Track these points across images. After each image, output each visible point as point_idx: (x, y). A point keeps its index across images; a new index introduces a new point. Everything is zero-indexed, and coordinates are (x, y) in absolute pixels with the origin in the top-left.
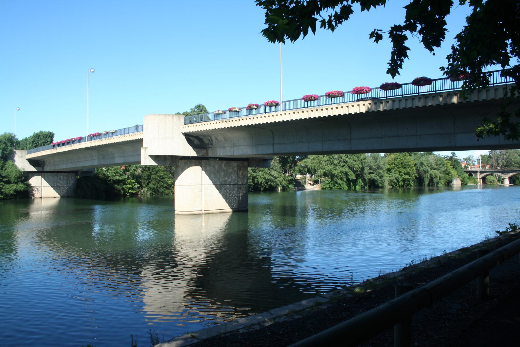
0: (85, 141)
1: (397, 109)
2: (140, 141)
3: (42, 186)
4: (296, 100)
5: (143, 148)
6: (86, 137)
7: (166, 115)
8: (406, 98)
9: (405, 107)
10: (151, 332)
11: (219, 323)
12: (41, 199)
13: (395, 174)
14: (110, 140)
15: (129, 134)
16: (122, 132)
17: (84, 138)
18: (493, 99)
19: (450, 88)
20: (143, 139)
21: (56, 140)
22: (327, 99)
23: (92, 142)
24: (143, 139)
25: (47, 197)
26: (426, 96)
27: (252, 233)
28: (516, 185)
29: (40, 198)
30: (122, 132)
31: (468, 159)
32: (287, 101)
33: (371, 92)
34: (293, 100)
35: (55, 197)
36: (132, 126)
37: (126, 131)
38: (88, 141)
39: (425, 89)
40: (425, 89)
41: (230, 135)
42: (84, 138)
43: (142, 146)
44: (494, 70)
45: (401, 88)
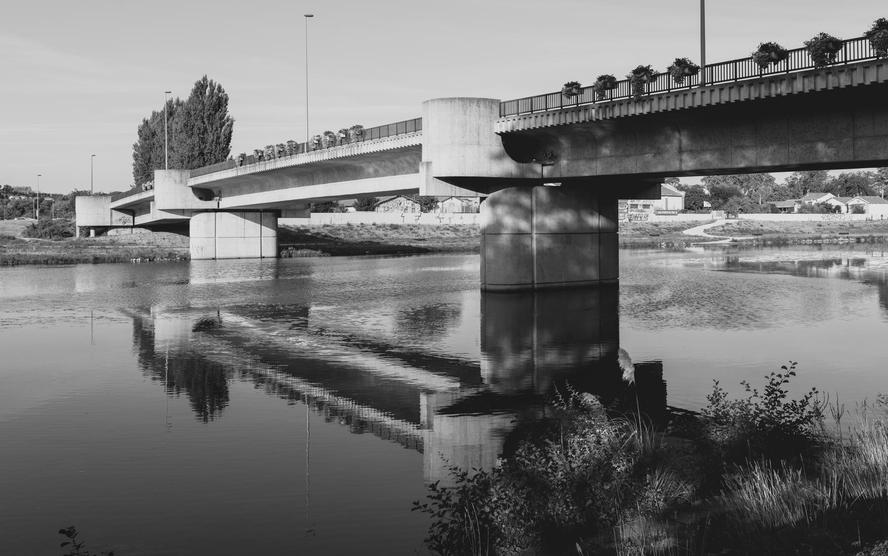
0: (303, 152)
1: (799, 92)
2: (419, 148)
4: (735, 61)
5: (423, 164)
6: (303, 144)
7: (471, 100)
8: (720, 87)
11: (143, 231)
12: (214, 261)
13: (833, 235)
14: (381, 143)
15: (388, 137)
16: (376, 133)
17: (301, 146)
19: (871, 56)
20: (421, 145)
22: (807, 57)
24: (421, 145)
25: (225, 258)
26: (776, 80)
29: (213, 259)
30: (376, 133)
33: (843, 49)
34: (730, 62)
36: (387, 124)
37: (385, 132)
38: (308, 152)
42: (301, 146)
43: (421, 161)
44: (846, 39)
45: (697, 75)
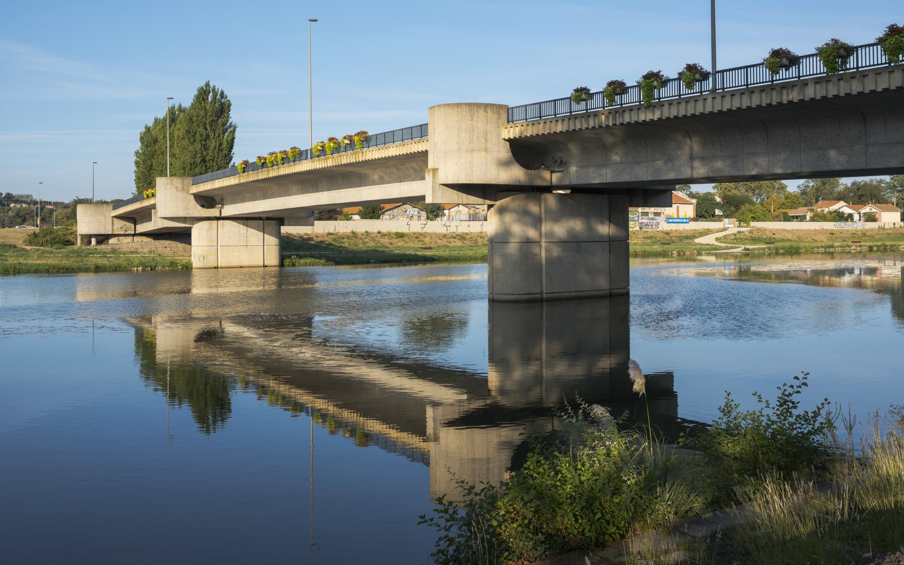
0: (307, 158)
2: (425, 154)
3: (219, 244)
4: (747, 67)
6: (307, 151)
8: (740, 92)
9: (836, 94)
10: (767, 446)
17: (304, 153)
18: (901, 87)
20: (427, 151)
21: (237, 160)
22: (818, 63)
23: (371, 150)
24: (427, 151)
27: (862, 281)
28: (436, 262)
29: (215, 268)
31: (872, 181)
32: (558, 100)
33: (855, 55)
35: (241, 267)
39: (786, 75)
40: (786, 75)
41: (261, 185)
42: (304, 153)
